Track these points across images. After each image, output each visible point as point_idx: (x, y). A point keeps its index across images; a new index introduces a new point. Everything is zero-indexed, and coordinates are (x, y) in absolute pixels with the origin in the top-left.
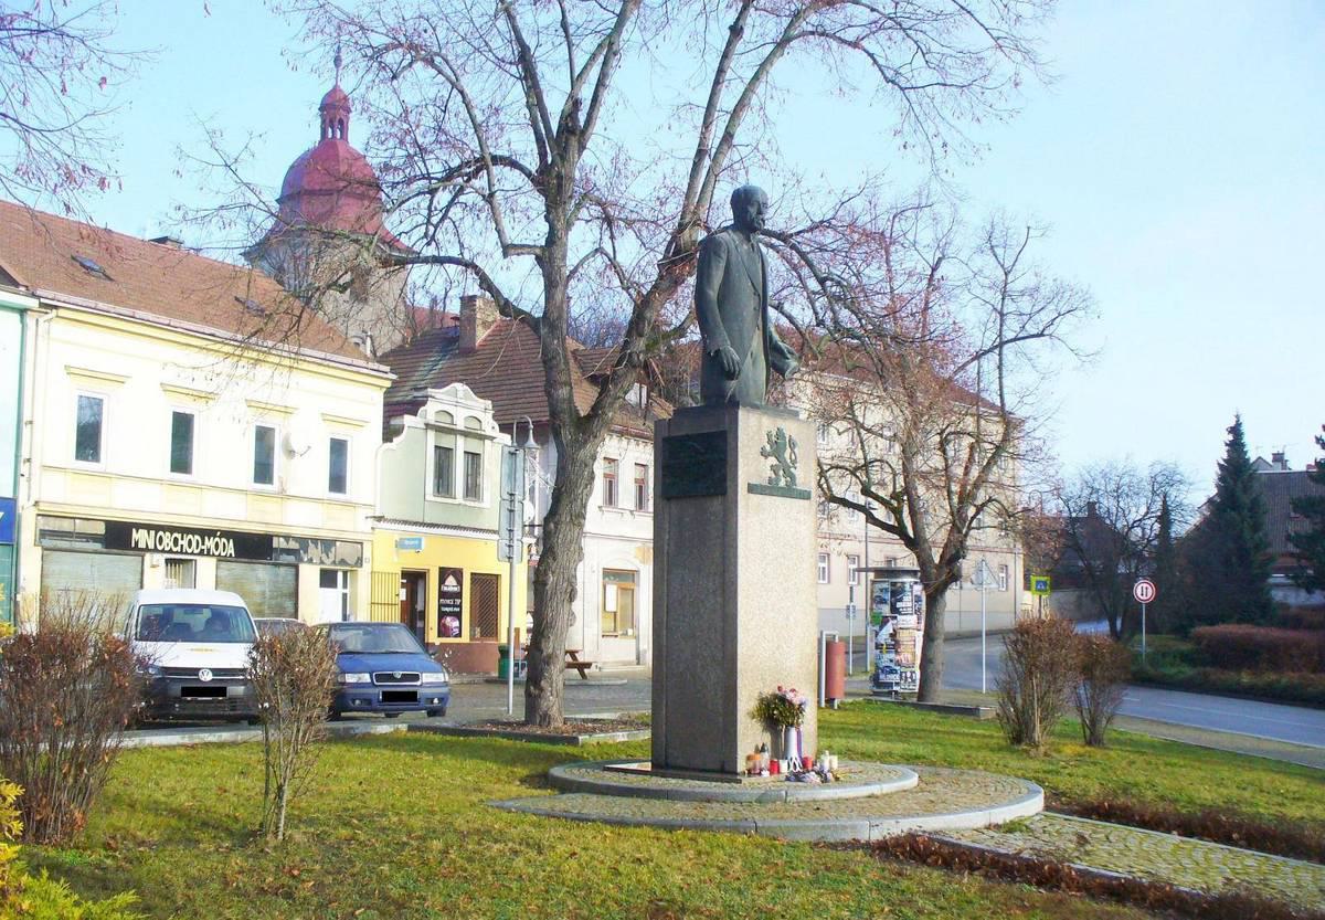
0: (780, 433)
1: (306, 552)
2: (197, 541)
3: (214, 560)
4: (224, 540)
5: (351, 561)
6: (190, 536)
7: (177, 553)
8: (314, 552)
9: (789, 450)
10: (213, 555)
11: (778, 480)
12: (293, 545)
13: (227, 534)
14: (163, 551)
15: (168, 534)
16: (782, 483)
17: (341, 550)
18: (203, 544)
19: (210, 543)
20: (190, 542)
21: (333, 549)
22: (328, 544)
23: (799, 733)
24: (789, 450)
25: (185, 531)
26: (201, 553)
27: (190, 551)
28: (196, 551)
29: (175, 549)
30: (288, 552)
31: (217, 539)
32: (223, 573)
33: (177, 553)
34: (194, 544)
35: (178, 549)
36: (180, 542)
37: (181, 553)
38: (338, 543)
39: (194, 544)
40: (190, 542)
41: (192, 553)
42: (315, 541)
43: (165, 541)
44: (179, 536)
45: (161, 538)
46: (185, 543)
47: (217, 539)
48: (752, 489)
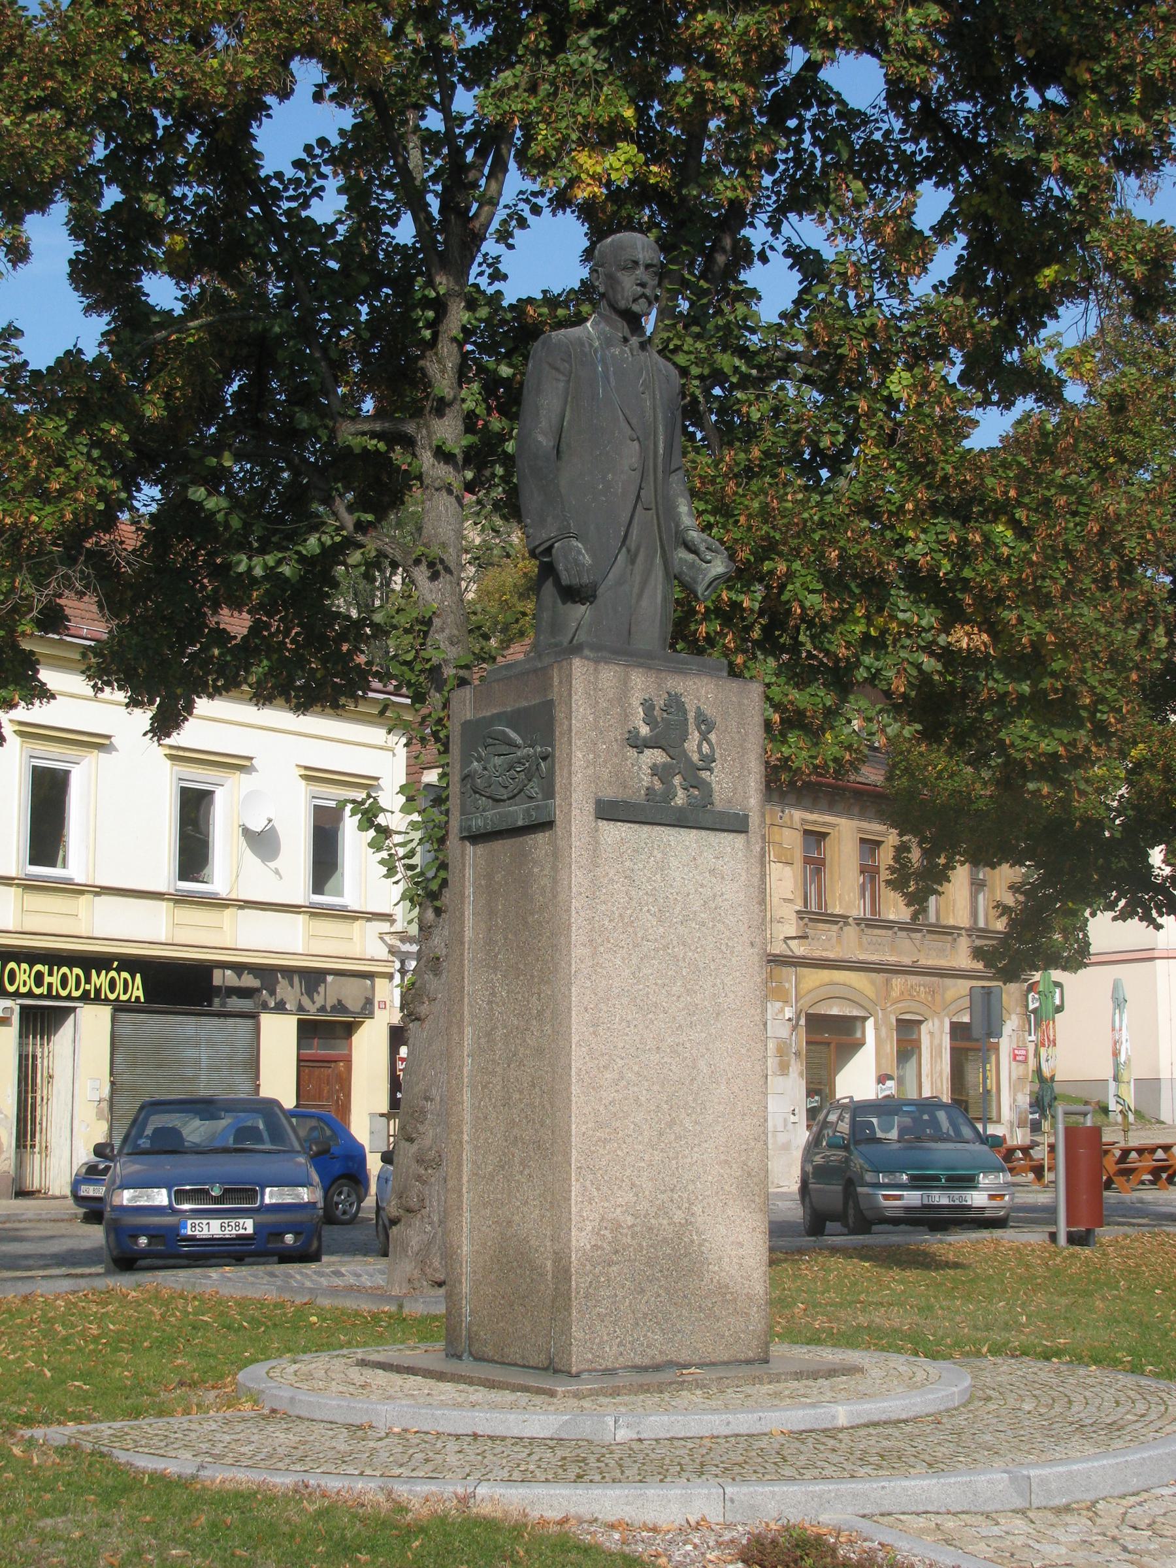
0: (675, 703)
1: (272, 993)
2: (78, 976)
3: (106, 1012)
4: (125, 975)
5: (354, 1005)
6: (65, 970)
7: (41, 996)
8: (288, 992)
9: (695, 736)
10: (107, 999)
11: (669, 794)
12: (249, 981)
13: (131, 964)
14: (17, 994)
15: (24, 966)
16: (680, 799)
17: (332, 990)
18: (88, 981)
19: (100, 980)
20: (64, 977)
21: (321, 989)
22: (312, 978)
23: (98, 1275)
24: (695, 736)
25: (54, 959)
26: (85, 997)
27: (64, 993)
28: (76, 994)
29: (37, 991)
30: (245, 993)
31: (113, 974)
32: (125, 1029)
33: (41, 996)
34: (72, 982)
35: (43, 990)
36: (47, 979)
37: (49, 996)
38: (330, 978)
39: (72, 982)
40: (64, 982)
41: (69, 998)
42: (289, 972)
43: (21, 977)
44: (44, 969)
45: (12, 972)
46: (55, 980)
47: (113, 974)
48: (608, 811)
